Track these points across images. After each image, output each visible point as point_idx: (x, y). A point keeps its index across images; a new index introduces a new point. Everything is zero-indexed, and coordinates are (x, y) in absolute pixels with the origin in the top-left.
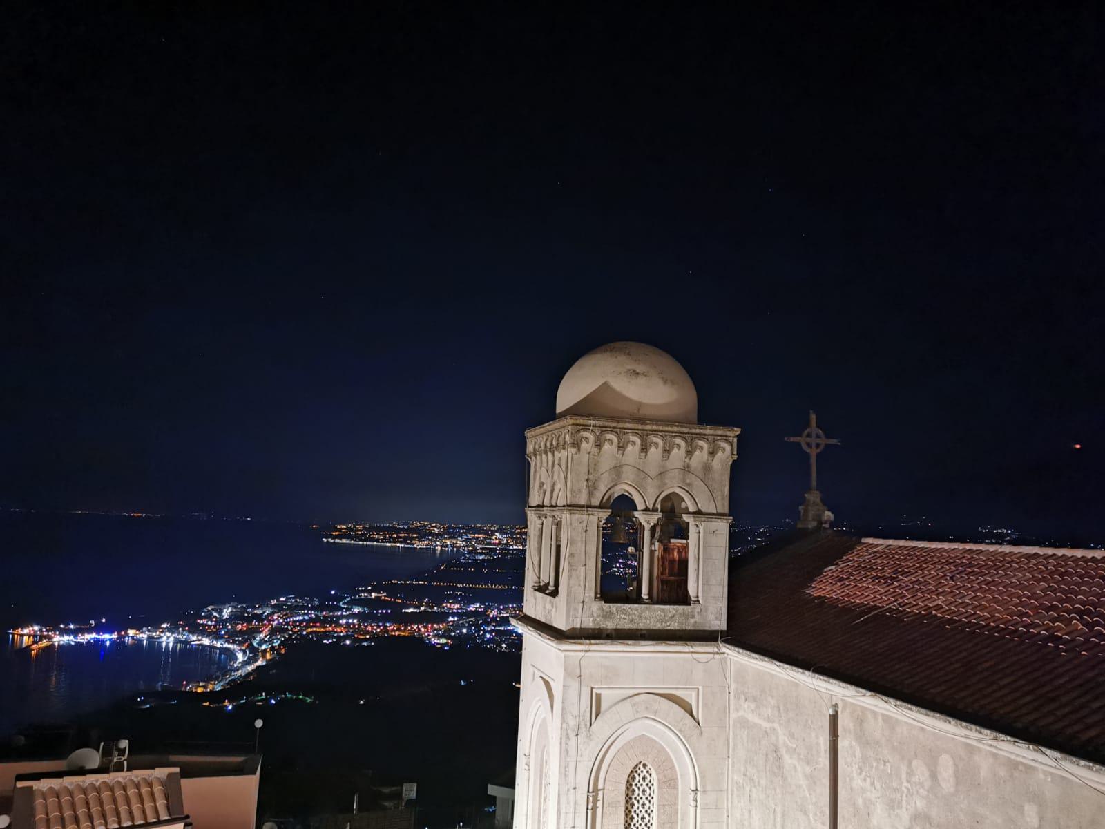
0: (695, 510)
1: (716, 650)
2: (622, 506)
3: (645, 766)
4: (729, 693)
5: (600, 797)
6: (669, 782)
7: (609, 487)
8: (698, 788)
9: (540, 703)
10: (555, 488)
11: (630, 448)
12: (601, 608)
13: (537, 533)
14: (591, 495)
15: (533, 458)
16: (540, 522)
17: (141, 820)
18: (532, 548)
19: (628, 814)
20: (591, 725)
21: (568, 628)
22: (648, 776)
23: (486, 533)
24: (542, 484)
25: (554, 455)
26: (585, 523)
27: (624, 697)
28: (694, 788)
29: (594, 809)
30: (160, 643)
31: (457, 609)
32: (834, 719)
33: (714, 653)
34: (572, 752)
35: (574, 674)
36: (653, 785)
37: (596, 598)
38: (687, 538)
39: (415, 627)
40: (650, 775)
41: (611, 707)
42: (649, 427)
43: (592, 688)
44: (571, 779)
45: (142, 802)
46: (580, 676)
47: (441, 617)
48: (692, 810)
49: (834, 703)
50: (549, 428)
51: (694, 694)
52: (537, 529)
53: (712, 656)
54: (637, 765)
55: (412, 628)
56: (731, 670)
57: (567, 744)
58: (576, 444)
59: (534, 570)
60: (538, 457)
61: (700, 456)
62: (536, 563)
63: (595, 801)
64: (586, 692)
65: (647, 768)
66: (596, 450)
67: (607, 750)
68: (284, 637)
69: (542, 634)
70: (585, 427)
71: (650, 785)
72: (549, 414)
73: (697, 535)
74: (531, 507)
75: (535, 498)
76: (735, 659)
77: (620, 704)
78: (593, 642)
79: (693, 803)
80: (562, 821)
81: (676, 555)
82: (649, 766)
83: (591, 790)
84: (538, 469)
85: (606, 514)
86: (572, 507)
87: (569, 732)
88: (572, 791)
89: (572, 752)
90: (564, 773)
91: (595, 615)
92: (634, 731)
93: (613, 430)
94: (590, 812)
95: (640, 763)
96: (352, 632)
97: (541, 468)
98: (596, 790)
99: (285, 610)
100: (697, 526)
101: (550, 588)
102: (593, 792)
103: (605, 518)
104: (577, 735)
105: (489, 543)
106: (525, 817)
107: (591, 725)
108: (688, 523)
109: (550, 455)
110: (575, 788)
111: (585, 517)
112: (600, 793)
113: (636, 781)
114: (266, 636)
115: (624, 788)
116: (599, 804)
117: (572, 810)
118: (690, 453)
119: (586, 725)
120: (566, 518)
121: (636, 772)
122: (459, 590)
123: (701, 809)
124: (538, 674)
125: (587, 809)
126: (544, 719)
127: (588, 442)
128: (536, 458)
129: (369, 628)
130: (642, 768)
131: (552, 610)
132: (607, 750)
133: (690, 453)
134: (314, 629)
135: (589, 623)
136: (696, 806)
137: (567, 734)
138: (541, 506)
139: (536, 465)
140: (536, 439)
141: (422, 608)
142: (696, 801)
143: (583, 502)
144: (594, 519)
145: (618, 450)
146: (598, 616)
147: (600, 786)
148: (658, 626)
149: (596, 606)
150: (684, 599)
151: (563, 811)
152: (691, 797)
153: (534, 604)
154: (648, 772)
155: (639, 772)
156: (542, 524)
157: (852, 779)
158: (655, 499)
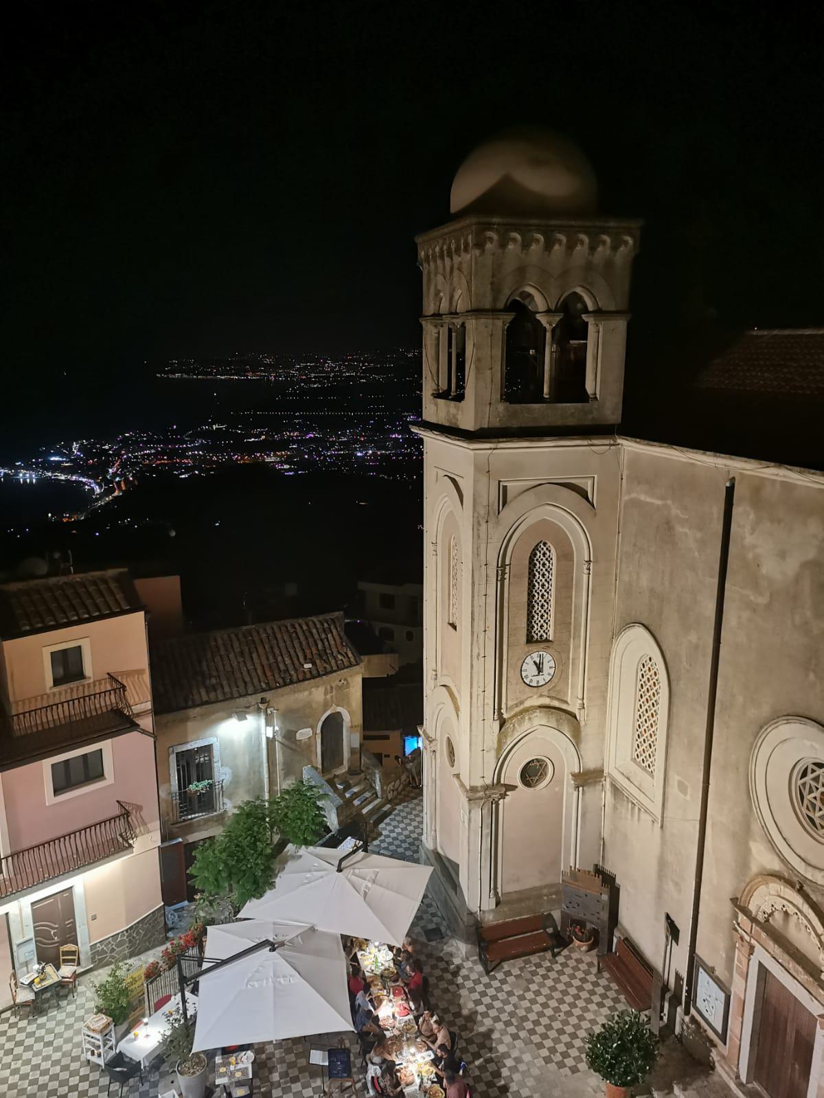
0: (595, 309)
1: (612, 442)
2: (519, 310)
3: (545, 544)
4: (622, 479)
5: (507, 571)
6: (566, 556)
7: (513, 289)
8: (592, 559)
9: (447, 499)
10: (455, 294)
11: (534, 247)
12: (506, 409)
13: (434, 342)
14: (495, 299)
15: (425, 265)
16: (436, 331)
17: (96, 611)
18: (429, 356)
19: (531, 585)
20: (499, 513)
21: (478, 427)
22: (548, 553)
23: (317, 361)
24: (437, 293)
25: (452, 260)
26: (491, 327)
27: (528, 488)
28: (587, 559)
29: (503, 579)
30: (19, 480)
31: (297, 436)
32: (730, 492)
33: (611, 445)
34: (483, 536)
35: (484, 470)
36: (551, 559)
37: (501, 399)
38: (586, 338)
39: (258, 455)
40: (550, 551)
41: (516, 497)
42: (553, 222)
43: (500, 481)
44: (483, 557)
45: (103, 596)
46: (489, 471)
47: (283, 445)
48: (585, 577)
49: (731, 477)
50: (446, 230)
51: (590, 482)
52: (434, 338)
53: (608, 447)
54: (538, 544)
55: (256, 456)
56: (625, 458)
57: (478, 530)
58: (480, 245)
59: (432, 378)
60: (432, 264)
61: (603, 251)
62: (434, 371)
63: (504, 573)
64: (494, 485)
65: (547, 546)
66: (500, 251)
67: (513, 533)
68: (136, 470)
69: (449, 436)
70: (489, 226)
71: (549, 559)
72: (440, 215)
73: (596, 334)
74: (427, 316)
75: (429, 307)
76: (630, 448)
77: (526, 493)
78: (501, 440)
79: (586, 571)
80: (476, 590)
81: (572, 356)
82: (549, 544)
83: (499, 566)
84: (432, 276)
85: (509, 317)
86: (477, 312)
87: (480, 519)
88: (484, 567)
89: (483, 536)
90: (476, 553)
91: (501, 415)
92: (533, 517)
93: (516, 228)
94: (499, 583)
95: (541, 542)
96: (199, 462)
97: (436, 275)
98: (504, 565)
99: (131, 445)
100: (597, 325)
101: (452, 394)
102: (501, 567)
103: (509, 320)
104: (487, 522)
105: (323, 372)
106: (435, 592)
107: (499, 513)
108: (587, 323)
109: (447, 260)
110: (486, 565)
111: (490, 321)
112: (508, 567)
113: (537, 557)
114: (118, 470)
115: (527, 562)
116: (507, 576)
117: (484, 582)
118: (593, 249)
119: (495, 513)
120: (471, 324)
121: (538, 550)
122: (297, 418)
123: (593, 576)
124: (442, 473)
125: (497, 580)
126: (451, 512)
127: (491, 243)
128: (429, 265)
129: (215, 458)
130: (542, 546)
131: (457, 414)
132: (513, 533)
133: (593, 249)
134: (163, 461)
135: (496, 423)
136: (589, 574)
137: (479, 522)
138: (437, 315)
139: (429, 272)
140: (428, 247)
141: (263, 437)
142: (589, 569)
143: (488, 306)
144: (499, 323)
145: (522, 250)
146: (503, 416)
147: (507, 562)
148: (559, 423)
149: (501, 407)
150: (582, 397)
151: (476, 583)
152: (585, 566)
153: (433, 410)
154: (547, 549)
155: (540, 549)
156: (439, 333)
157: (743, 538)
158: (557, 300)
